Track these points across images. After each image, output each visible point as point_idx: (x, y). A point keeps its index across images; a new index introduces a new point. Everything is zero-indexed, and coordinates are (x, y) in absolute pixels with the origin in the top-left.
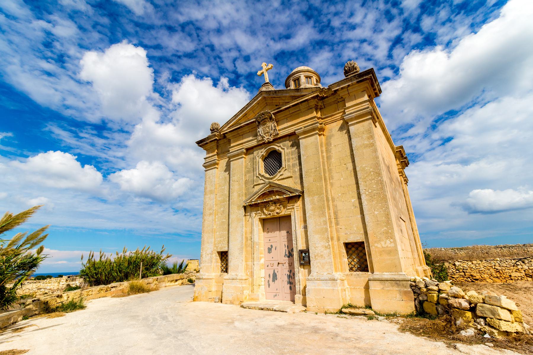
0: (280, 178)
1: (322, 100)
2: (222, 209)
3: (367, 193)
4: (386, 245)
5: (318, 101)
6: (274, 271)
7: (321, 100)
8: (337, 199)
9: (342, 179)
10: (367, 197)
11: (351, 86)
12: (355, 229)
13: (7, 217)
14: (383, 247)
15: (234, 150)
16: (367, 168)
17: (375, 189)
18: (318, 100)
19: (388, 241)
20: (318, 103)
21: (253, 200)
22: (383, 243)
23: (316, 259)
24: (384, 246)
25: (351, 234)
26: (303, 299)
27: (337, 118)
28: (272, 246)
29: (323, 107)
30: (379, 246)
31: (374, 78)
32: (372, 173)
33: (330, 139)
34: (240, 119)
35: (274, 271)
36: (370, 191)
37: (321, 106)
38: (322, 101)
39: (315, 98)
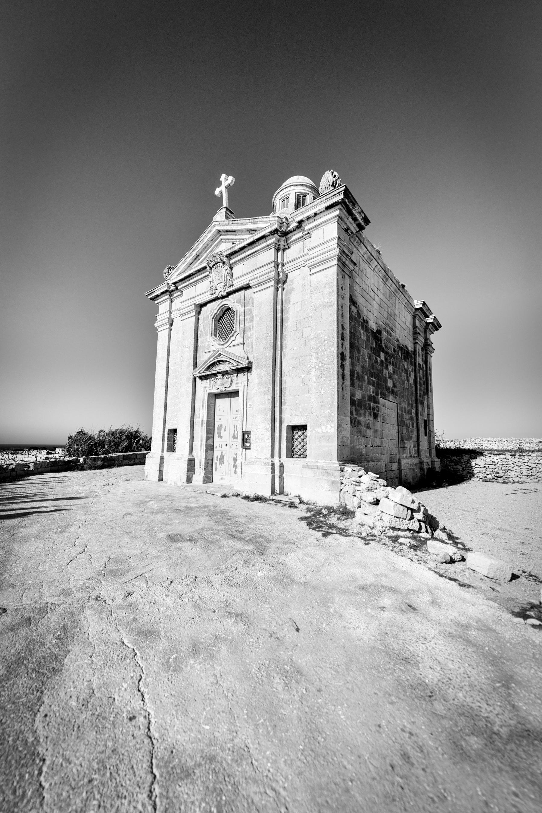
0: (231, 345)
1: (285, 236)
2: (174, 381)
3: (317, 367)
4: (326, 430)
5: (279, 237)
6: (222, 453)
7: (283, 236)
8: (288, 374)
9: (296, 348)
10: (316, 373)
11: (319, 214)
12: (301, 410)
13: (342, 208)
14: (323, 432)
15: (315, 255)
16: (321, 336)
17: (326, 363)
18: (279, 236)
19: (329, 426)
20: (279, 240)
21: (202, 372)
22: (323, 427)
23: (257, 442)
24: (324, 431)
25: (295, 415)
26: (419, 491)
27: (301, 263)
28: (221, 425)
29: (287, 247)
30: (319, 430)
31: (351, 202)
32: (326, 342)
33: (290, 293)
34: (191, 262)
35: (222, 453)
36: (320, 365)
37: (284, 246)
38: (284, 238)
39: (274, 234)
